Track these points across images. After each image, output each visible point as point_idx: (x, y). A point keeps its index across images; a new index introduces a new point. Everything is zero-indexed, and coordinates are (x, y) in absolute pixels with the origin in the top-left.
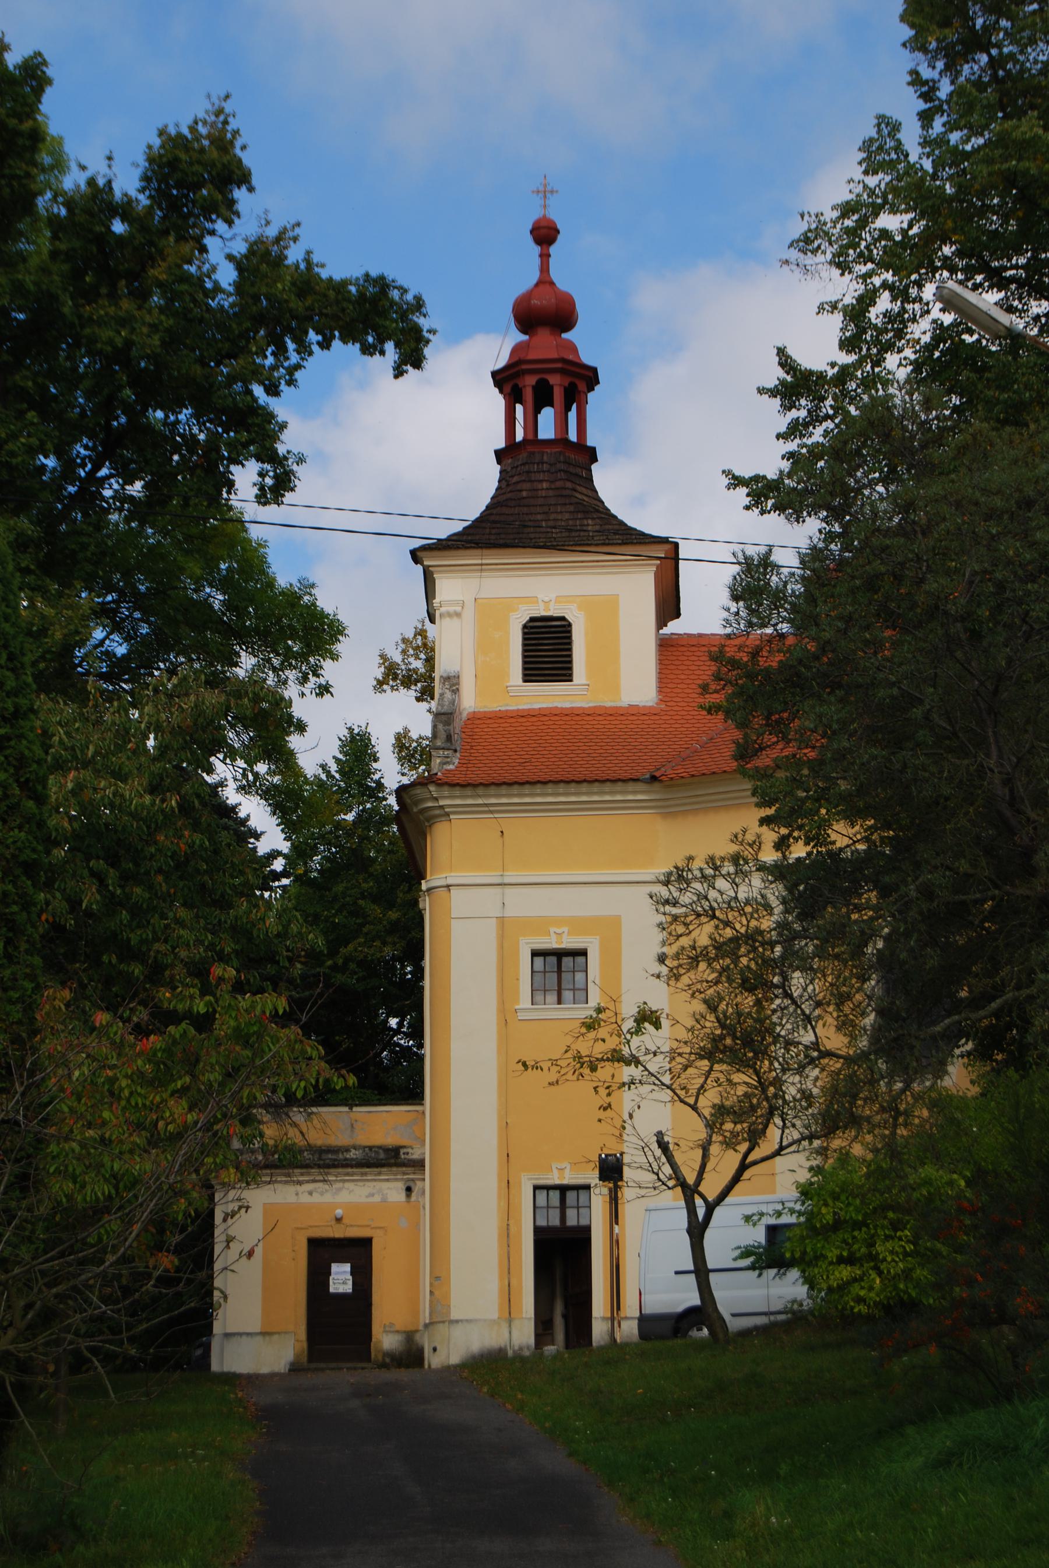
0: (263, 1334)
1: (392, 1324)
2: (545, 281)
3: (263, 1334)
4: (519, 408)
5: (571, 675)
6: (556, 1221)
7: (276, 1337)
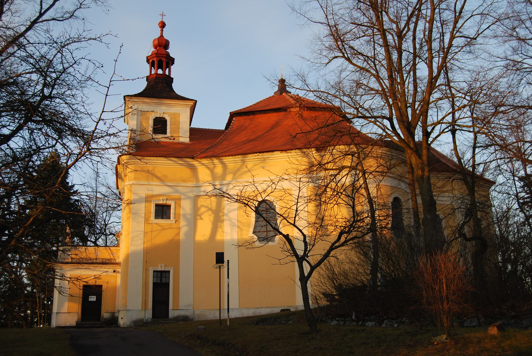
0: (67, 313)
2: (162, 36)
3: (67, 313)
6: (159, 281)
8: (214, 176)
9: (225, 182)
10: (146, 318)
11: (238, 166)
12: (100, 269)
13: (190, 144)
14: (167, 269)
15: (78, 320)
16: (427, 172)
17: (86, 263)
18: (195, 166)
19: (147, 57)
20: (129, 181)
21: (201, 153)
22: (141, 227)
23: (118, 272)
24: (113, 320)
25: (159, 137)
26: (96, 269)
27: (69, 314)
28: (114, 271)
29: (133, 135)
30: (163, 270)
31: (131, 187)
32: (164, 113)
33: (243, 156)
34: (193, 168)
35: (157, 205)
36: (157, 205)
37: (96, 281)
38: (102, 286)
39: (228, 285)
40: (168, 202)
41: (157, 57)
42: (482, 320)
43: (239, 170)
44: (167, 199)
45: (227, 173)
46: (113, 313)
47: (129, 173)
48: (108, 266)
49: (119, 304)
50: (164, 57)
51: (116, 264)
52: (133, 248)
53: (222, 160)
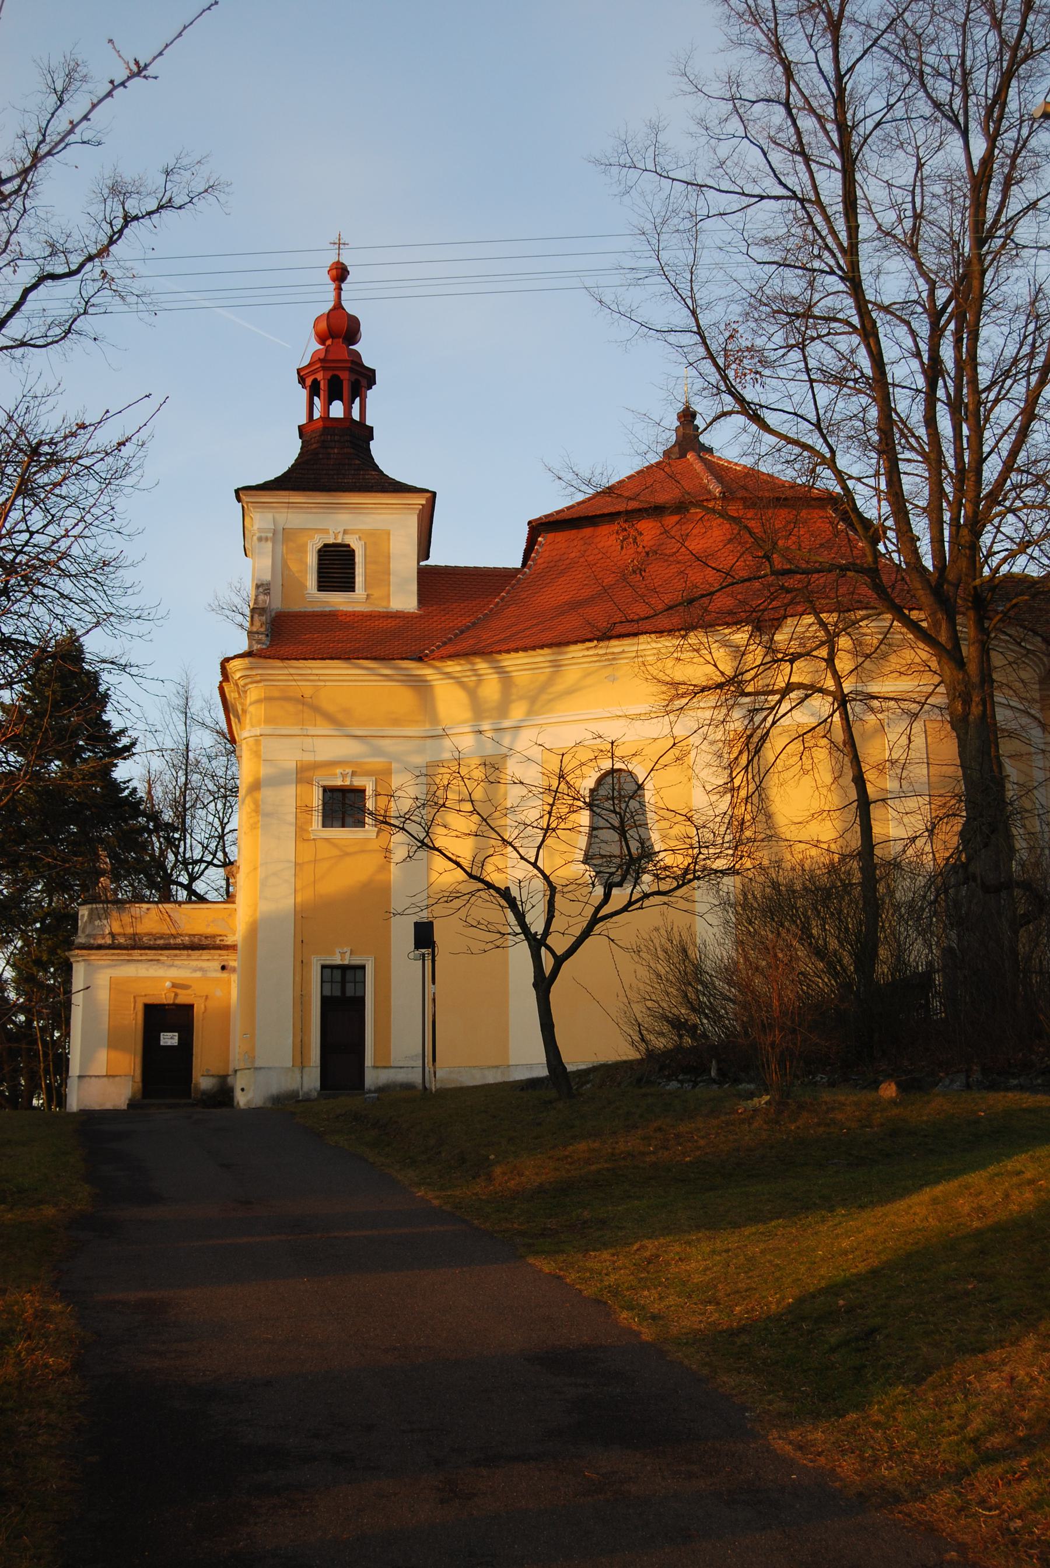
1: (208, 1070)
2: (338, 306)
4: (316, 399)
5: (354, 587)
6: (337, 993)
7: (117, 1079)
8: (478, 710)
9: (506, 724)
10: (305, 1089)
11: (543, 678)
12: (186, 962)
13: (421, 616)
14: (356, 961)
15: (134, 1094)
16: (977, 705)
17: (150, 948)
18: (426, 681)
19: (299, 371)
20: (252, 726)
21: (445, 643)
22: (287, 849)
23: (234, 970)
24: (223, 1095)
25: (337, 601)
26: (176, 963)
27: (111, 1079)
28: (223, 968)
29: (261, 597)
30: (346, 962)
31: (257, 742)
32: (345, 532)
33: (555, 649)
34: (422, 688)
35: (326, 790)
36: (326, 790)
37: (176, 995)
38: (191, 1006)
39: (434, 1000)
40: (358, 782)
41: (324, 369)
42: (976, 1076)
43: (543, 688)
44: (353, 774)
45: (514, 697)
46: (223, 1078)
47: (251, 704)
48: (205, 954)
49: (237, 1056)
50: (343, 369)
51: (227, 947)
52: (265, 907)
53: (499, 661)
